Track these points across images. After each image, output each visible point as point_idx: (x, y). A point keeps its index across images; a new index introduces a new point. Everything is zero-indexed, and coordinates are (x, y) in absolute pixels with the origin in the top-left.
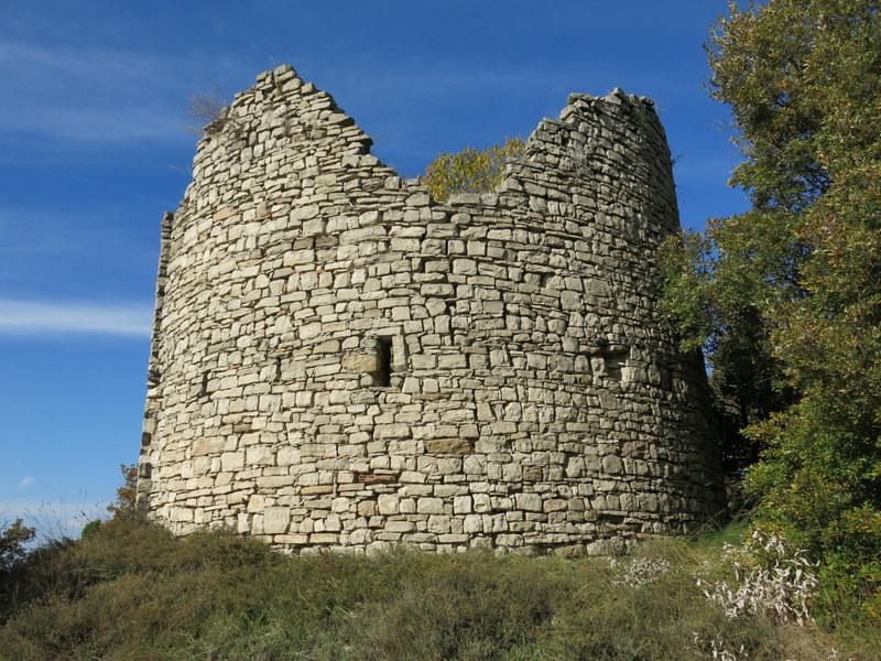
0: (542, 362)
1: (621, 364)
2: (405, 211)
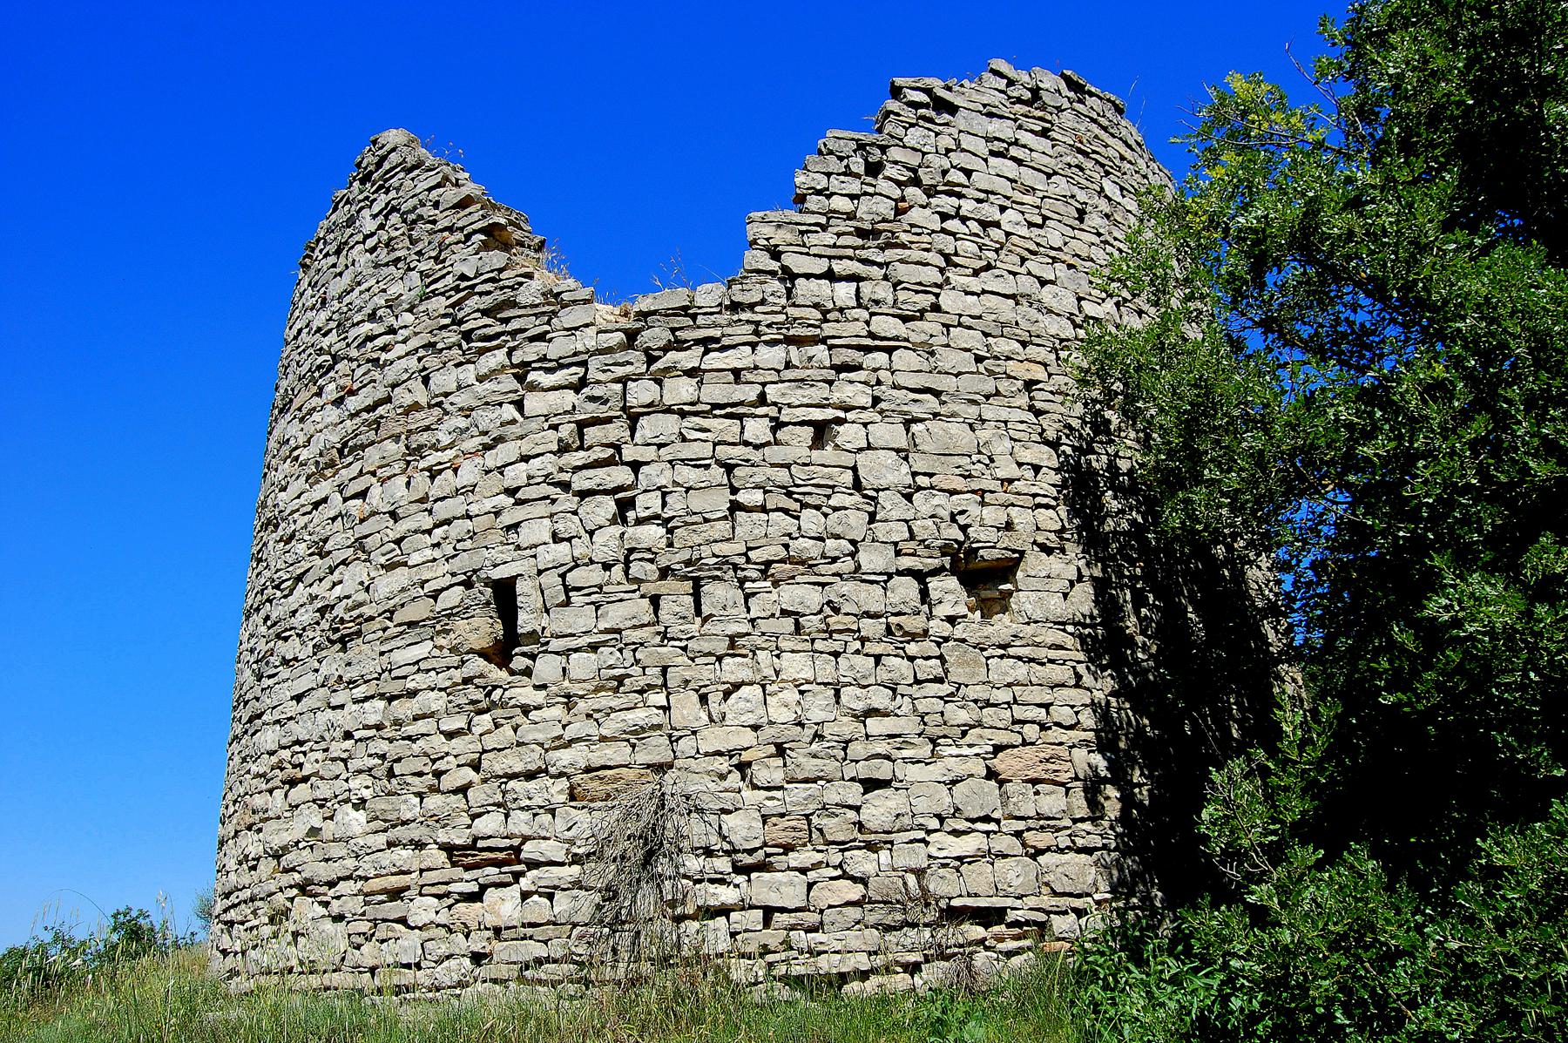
0: (815, 598)
1: (1008, 586)
2: (550, 340)
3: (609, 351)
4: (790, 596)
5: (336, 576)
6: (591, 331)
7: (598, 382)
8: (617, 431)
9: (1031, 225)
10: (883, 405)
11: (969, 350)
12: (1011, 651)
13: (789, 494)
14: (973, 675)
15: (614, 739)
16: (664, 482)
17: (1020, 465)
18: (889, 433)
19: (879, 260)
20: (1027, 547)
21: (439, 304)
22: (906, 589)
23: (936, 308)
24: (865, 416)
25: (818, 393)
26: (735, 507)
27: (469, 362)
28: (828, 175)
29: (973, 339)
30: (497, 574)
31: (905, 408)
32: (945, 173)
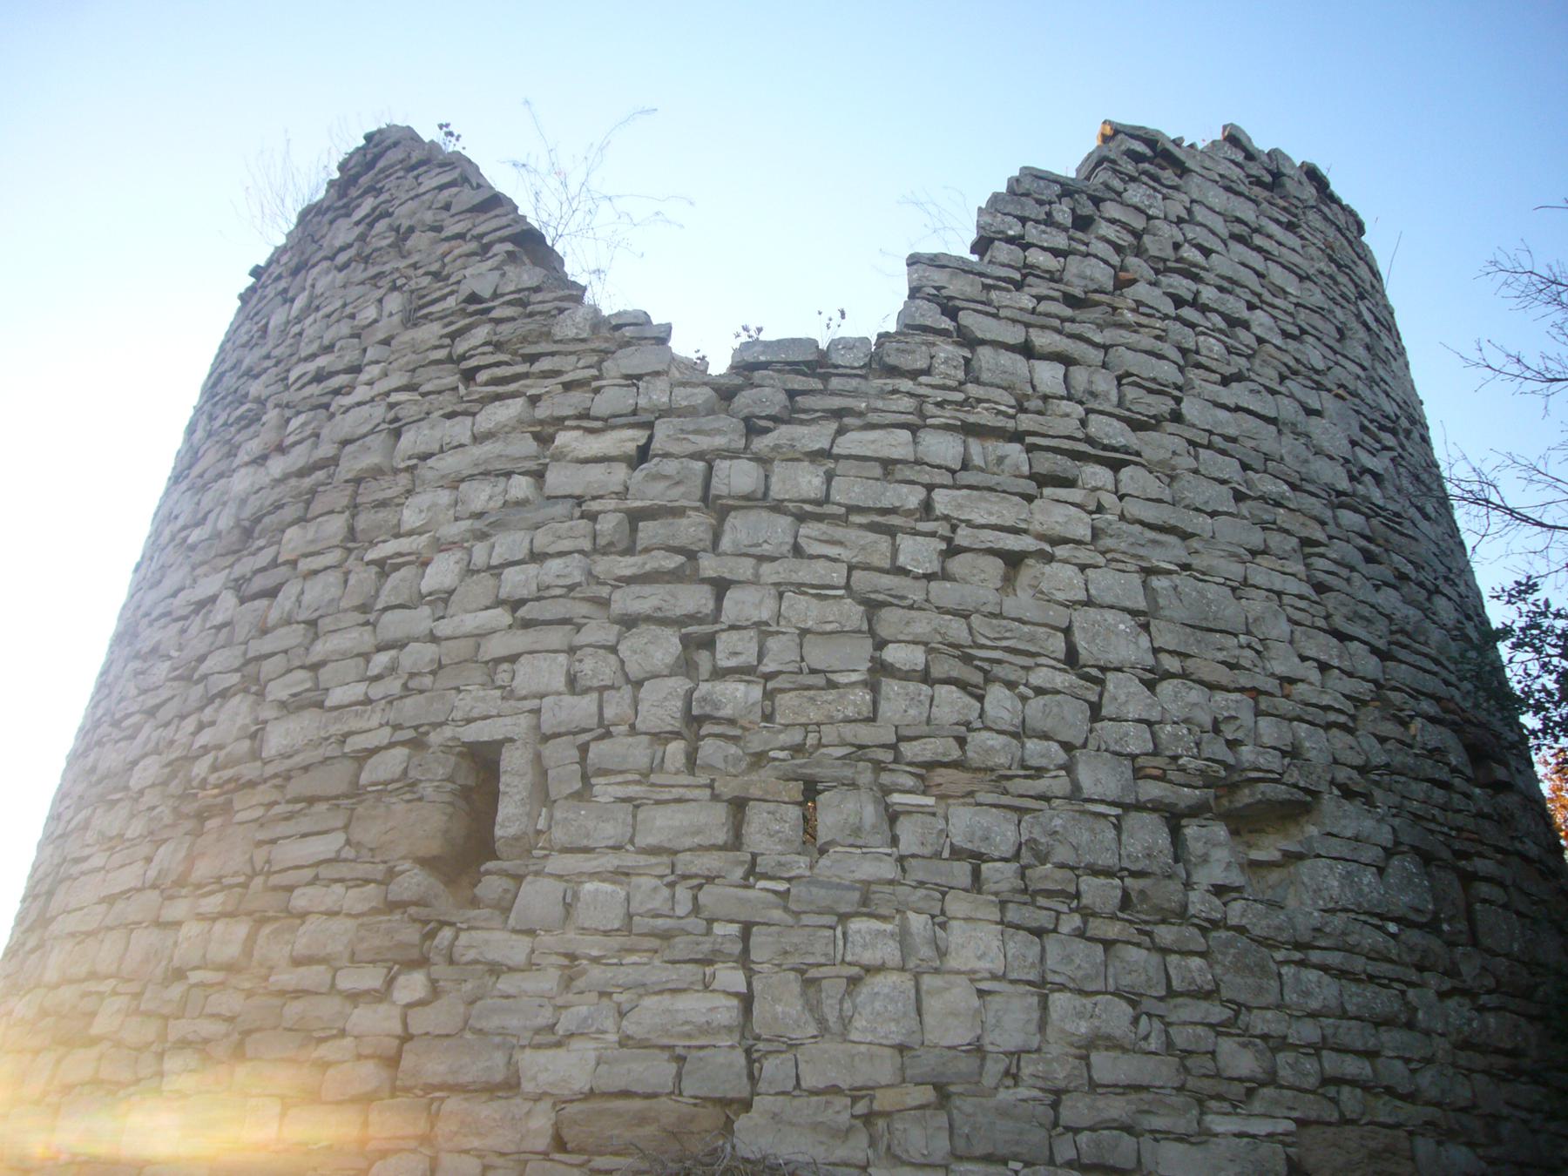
0: (1003, 833)
3: (691, 411)
4: (964, 823)
5: (208, 714)
6: (661, 384)
7: (666, 455)
8: (692, 529)
9: (1286, 335)
10: (1107, 542)
11: (1223, 482)
12: (1315, 956)
13: (967, 659)
14: (1260, 990)
15: (644, 1045)
16: (765, 616)
17: (1303, 659)
18: (1119, 585)
19: (1098, 339)
20: (1323, 787)
21: (431, 332)
22: (1147, 835)
23: (1177, 417)
24: (1084, 555)
25: (1010, 511)
26: (880, 669)
27: (466, 413)
28: (1023, 220)
29: (1230, 468)
30: (472, 733)
31: (1141, 551)
32: (1177, 246)
